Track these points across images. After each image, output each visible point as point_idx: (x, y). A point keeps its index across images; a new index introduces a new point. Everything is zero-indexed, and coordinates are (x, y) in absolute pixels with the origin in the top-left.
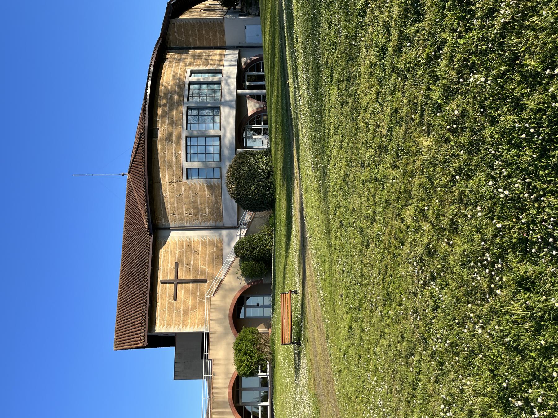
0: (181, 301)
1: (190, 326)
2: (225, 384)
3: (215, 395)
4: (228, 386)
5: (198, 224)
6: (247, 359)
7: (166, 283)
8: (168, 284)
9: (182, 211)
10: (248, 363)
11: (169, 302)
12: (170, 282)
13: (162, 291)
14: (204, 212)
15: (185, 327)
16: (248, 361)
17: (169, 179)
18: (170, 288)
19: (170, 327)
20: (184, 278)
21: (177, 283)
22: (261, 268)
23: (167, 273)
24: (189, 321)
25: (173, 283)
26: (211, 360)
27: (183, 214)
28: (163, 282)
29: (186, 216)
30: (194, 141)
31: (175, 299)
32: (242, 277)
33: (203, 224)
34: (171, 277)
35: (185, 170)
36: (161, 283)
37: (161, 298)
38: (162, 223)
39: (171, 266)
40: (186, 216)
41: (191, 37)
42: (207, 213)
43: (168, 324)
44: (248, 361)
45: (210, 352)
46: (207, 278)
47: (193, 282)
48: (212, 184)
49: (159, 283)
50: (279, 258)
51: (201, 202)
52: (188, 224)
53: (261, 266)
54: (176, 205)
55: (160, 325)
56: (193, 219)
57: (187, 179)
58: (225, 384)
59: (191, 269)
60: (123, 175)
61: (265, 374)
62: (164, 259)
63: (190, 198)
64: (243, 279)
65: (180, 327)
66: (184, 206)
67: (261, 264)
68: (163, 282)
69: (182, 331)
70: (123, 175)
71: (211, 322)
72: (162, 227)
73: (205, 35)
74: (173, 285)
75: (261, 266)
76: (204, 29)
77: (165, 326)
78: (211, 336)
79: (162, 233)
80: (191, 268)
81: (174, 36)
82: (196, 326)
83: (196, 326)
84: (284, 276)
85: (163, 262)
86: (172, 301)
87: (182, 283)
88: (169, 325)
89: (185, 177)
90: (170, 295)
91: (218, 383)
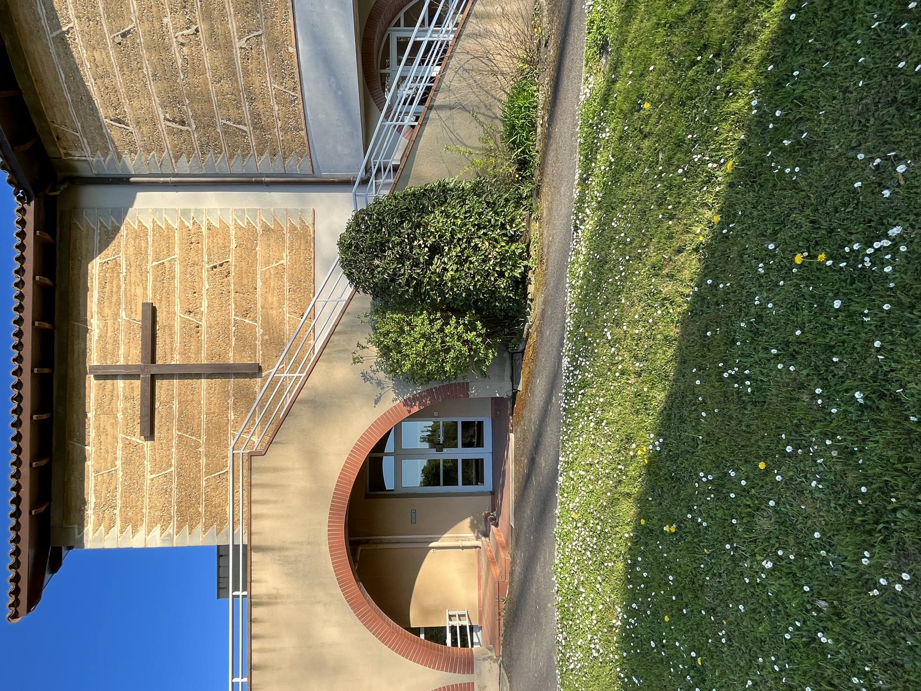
1: (206, 527)
5: (222, 164)
7: (114, 377)
8: (120, 383)
9: (150, 110)
11: (128, 444)
12: (129, 375)
13: (99, 405)
14: (233, 113)
18: (127, 391)
19: (191, 528)
20: (176, 360)
23: (116, 341)
24: (202, 509)
27: (154, 122)
28: (105, 375)
33: (237, 167)
36: (97, 377)
37: (98, 428)
38: (87, 158)
39: (130, 319)
43: (126, 522)
47: (210, 376)
52: (184, 166)
53: (471, 336)
55: (98, 523)
56: (196, 144)
62: (102, 287)
65: (169, 530)
66: (152, 88)
67: (471, 327)
68: (105, 375)
69: (177, 542)
72: (93, 173)
74: (137, 383)
75: (471, 336)
78: (255, 557)
79: (95, 198)
80: (204, 323)
85: (101, 302)
86: (138, 439)
87: (170, 376)
88: (132, 523)
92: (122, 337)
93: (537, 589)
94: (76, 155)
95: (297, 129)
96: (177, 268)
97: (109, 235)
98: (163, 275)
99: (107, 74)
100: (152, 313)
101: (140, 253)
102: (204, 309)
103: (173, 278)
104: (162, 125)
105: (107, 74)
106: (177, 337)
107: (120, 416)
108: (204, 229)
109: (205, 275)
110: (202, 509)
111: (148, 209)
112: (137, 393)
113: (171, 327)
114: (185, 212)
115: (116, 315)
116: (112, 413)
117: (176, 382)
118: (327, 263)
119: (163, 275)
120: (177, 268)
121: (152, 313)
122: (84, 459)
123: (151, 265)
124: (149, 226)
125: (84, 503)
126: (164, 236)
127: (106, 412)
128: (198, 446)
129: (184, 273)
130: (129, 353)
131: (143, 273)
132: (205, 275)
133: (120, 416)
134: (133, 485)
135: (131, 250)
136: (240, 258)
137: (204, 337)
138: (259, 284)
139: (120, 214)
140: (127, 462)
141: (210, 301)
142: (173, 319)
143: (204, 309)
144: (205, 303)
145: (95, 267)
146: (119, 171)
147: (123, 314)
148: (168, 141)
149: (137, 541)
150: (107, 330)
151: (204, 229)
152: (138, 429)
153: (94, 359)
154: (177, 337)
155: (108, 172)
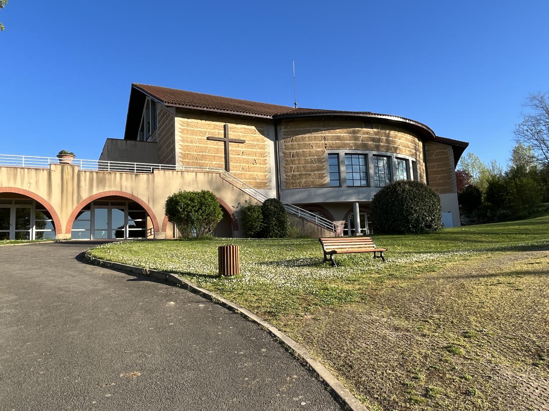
0: (207, 144)
2: (126, 187)
3: (113, 175)
4: (124, 190)
6: (195, 206)
8: (223, 132)
9: (295, 149)
10: (190, 207)
13: (217, 126)
15: (181, 147)
16: (193, 207)
17: (328, 136)
19: (180, 132)
21: (225, 142)
22: (256, 227)
23: (234, 132)
25: (225, 136)
26: (153, 173)
27: (293, 149)
29: (290, 153)
30: (362, 161)
31: (208, 139)
32: (239, 208)
34: (232, 135)
35: (337, 152)
36: (225, 126)
38: (282, 130)
40: (290, 153)
41: (436, 164)
42: (295, 173)
43: (183, 130)
44: (193, 207)
45: (162, 172)
46: (230, 172)
48: (325, 178)
49: (225, 124)
50: (399, 245)
51: (306, 167)
54: (302, 143)
56: (287, 159)
57: (329, 154)
58: (126, 187)
59: (238, 156)
60: (295, 104)
61: (128, 236)
62: (249, 129)
63: (310, 156)
64: (238, 210)
70: (295, 104)
71: (195, 173)
73: (439, 176)
76: (445, 175)
77: (181, 127)
80: (240, 156)
81: (435, 148)
82: (181, 159)
83: (181, 159)
84: (498, 250)
85: (245, 128)
86: (207, 135)
88: (182, 131)
89: (330, 152)
90: (213, 133)
91: (127, 179)
92: (236, 133)
93: (217, 240)
94: (283, 127)
95: (293, 186)
96: (254, 150)
97: (262, 133)
98: (253, 146)
99: (303, 140)
100: (243, 142)
101: (258, 140)
102: (244, 157)
103: (252, 148)
104: (292, 151)
105: (303, 140)
106: (236, 149)
107: (214, 131)
108: (265, 158)
109: (253, 158)
110: (186, 152)
111: (270, 144)
112: (220, 136)
113: (239, 147)
114: (269, 153)
115: (242, 132)
116: (214, 128)
117: (223, 147)
118: (267, 194)
119: (253, 146)
120: (254, 150)
121: (243, 142)
122: (201, 120)
123: (255, 143)
124: (265, 143)
125: (188, 119)
126: (263, 147)
127: (215, 128)
128: (205, 152)
129: (253, 152)
130: (232, 135)
131: (253, 140)
132: (253, 158)
133: (214, 131)
134: (193, 133)
135: (258, 138)
136: (258, 168)
137: (236, 156)
138: (251, 173)
139: (268, 136)
140: (200, 132)
141: (246, 159)
142: (241, 148)
143: (244, 157)
144: (245, 157)
145: (253, 128)
146: (279, 137)
147: (242, 134)
148: (287, 151)
149: (177, 132)
150: (237, 130)
151: (265, 158)
152: (210, 136)
153: (230, 125)
154: (236, 149)
155: (279, 134)
